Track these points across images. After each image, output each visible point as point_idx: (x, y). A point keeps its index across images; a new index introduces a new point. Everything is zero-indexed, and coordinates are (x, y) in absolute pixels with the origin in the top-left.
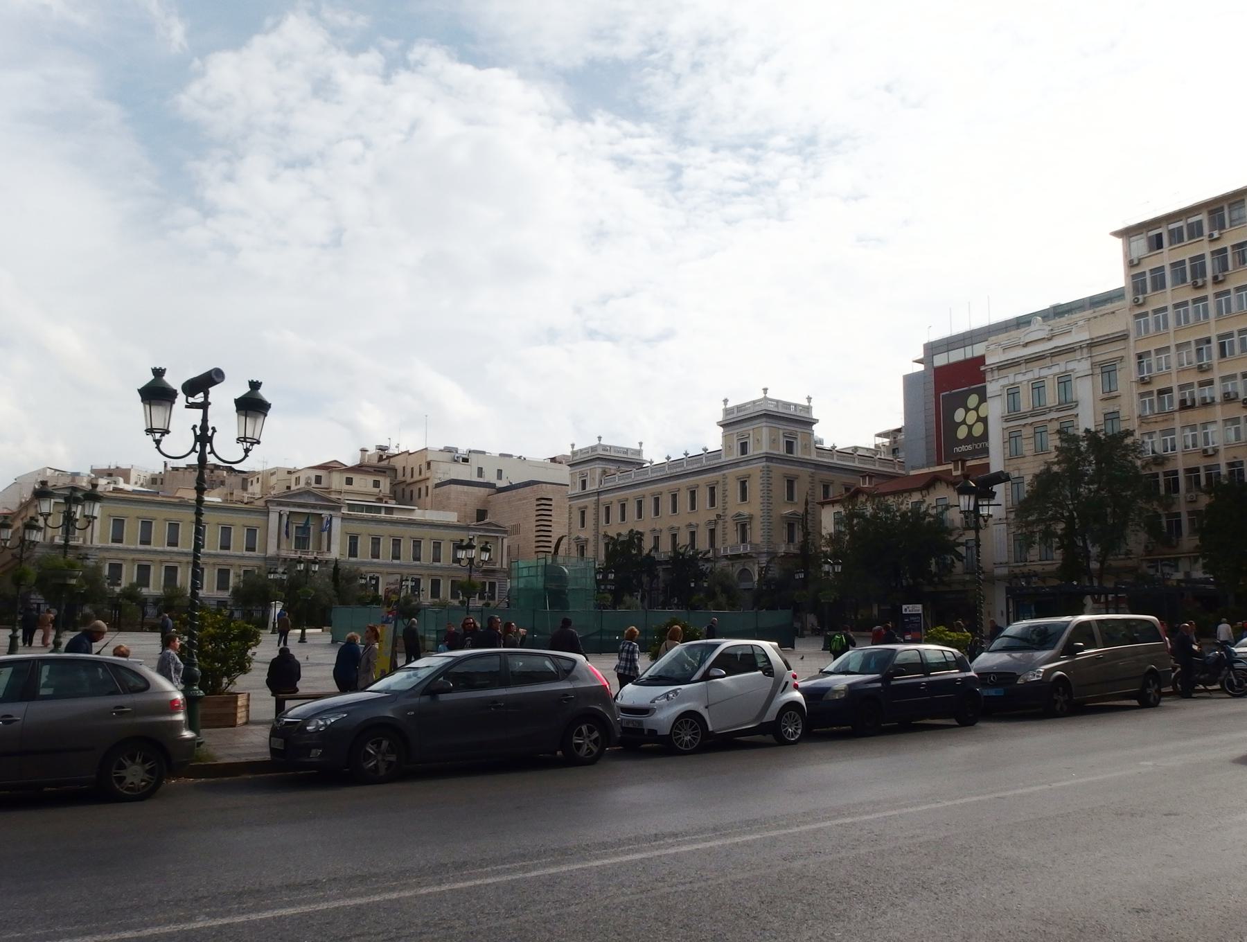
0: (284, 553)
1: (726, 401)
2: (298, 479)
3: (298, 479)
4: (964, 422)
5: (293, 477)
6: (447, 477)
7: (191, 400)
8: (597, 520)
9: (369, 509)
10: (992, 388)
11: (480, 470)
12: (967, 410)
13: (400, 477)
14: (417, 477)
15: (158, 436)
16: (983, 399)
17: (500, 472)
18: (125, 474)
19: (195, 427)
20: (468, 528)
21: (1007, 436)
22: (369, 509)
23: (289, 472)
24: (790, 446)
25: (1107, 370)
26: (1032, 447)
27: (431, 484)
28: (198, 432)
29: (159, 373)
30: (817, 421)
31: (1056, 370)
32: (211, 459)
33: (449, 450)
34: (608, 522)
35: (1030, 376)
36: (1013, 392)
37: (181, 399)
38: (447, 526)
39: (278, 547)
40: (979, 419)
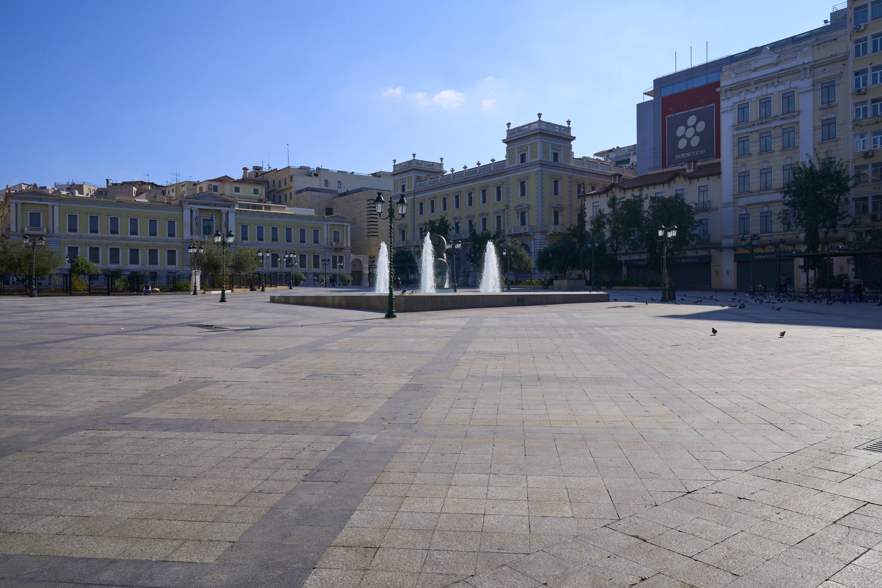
4: (684, 136)
9: (254, 207)
11: (326, 181)
12: (687, 127)
13: (271, 187)
14: (283, 186)
17: (339, 182)
18: (80, 188)
21: (736, 141)
22: (254, 207)
23: (195, 184)
25: (828, 88)
26: (758, 148)
27: (293, 191)
30: (574, 138)
31: (781, 88)
34: (421, 213)
36: (743, 108)
38: (309, 218)
39: (191, 234)
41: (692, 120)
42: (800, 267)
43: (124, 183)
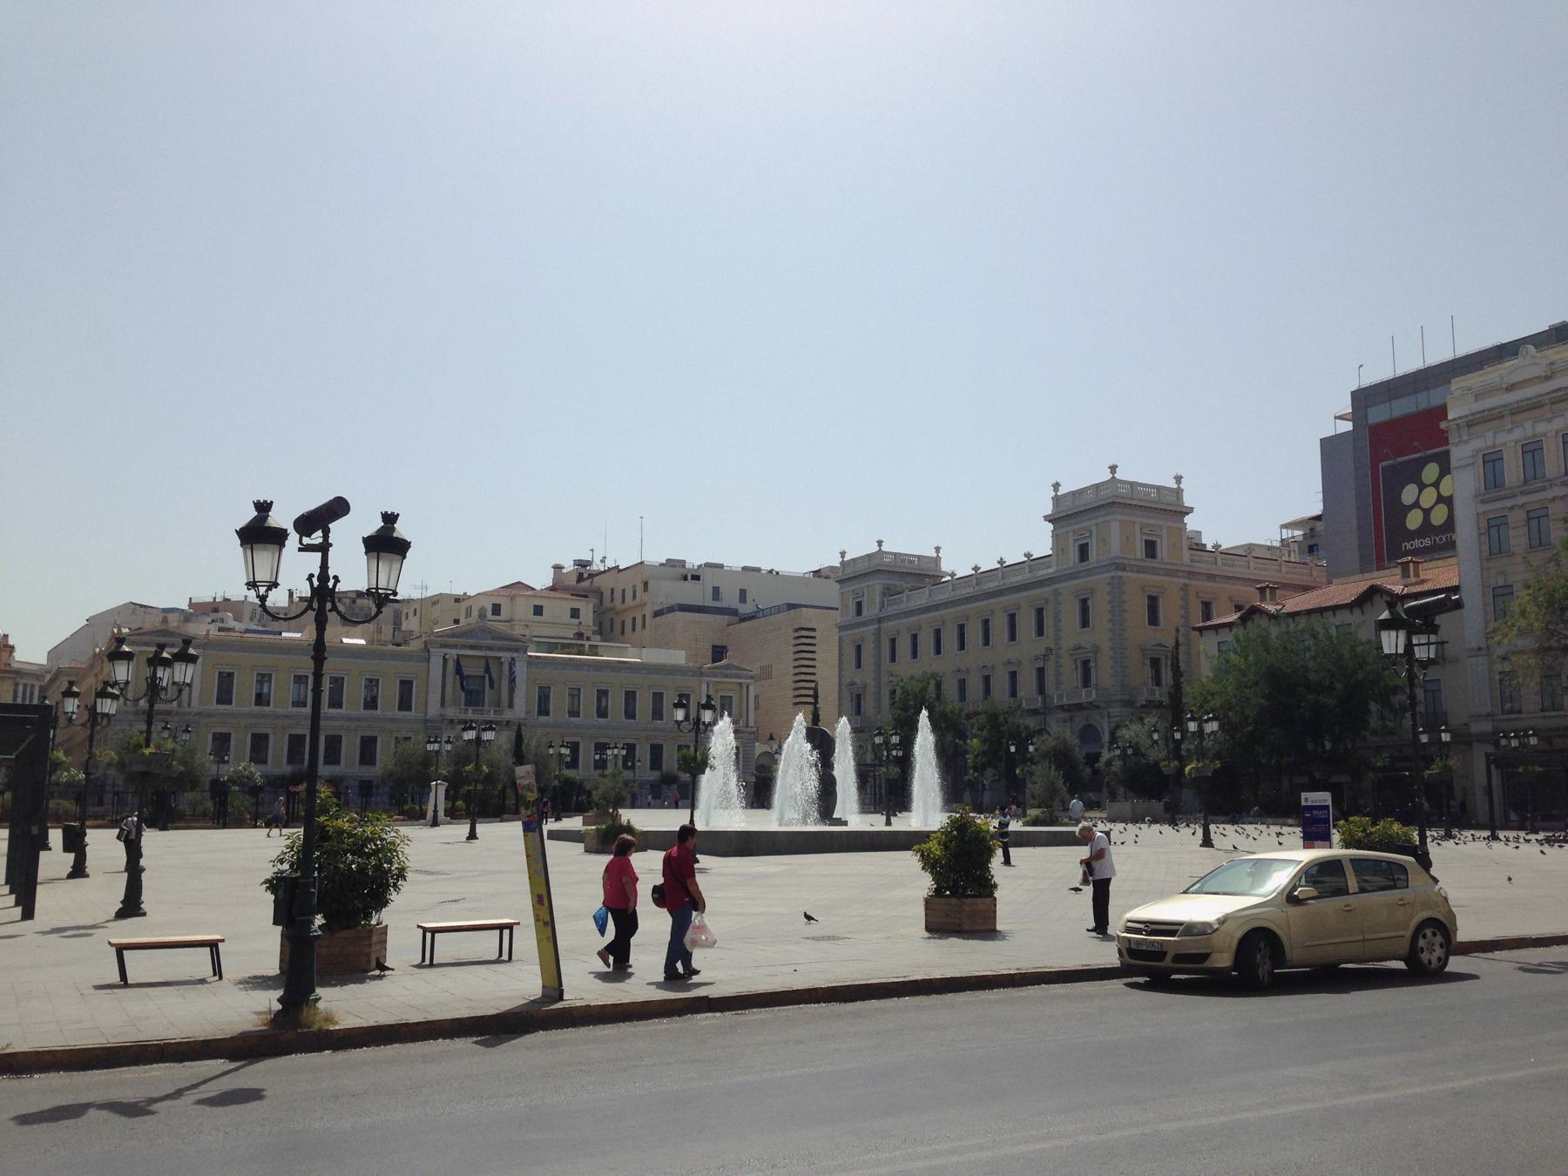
1: (1056, 486)
2: (469, 612)
3: (469, 612)
4: (1416, 505)
5: (463, 605)
6: (672, 602)
7: (306, 540)
8: (878, 655)
10: (1460, 453)
11: (716, 591)
12: (1422, 487)
15: (262, 590)
16: (1445, 470)
17: (743, 593)
19: (311, 576)
20: (700, 673)
21: (1484, 524)
22: (565, 648)
23: (457, 600)
24: (1151, 549)
26: (1524, 540)
28: (316, 583)
29: (263, 508)
30: (1191, 510)
33: (671, 563)
35: (1517, 434)
36: (1492, 461)
37: (293, 539)
39: (443, 704)
40: (1440, 499)
42: (888, 823)
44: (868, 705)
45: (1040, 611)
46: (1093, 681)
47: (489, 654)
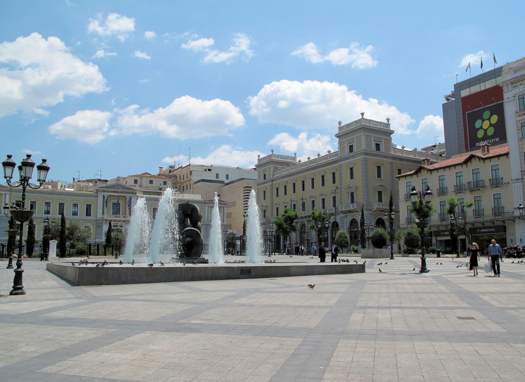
0: (106, 217)
4: (481, 128)
11: (217, 176)
12: (483, 120)
32: (421, 256)
39: (103, 214)
41: (487, 114)
43: (87, 180)
44: (268, 214)
45: (334, 174)
46: (355, 201)
47: (121, 194)
